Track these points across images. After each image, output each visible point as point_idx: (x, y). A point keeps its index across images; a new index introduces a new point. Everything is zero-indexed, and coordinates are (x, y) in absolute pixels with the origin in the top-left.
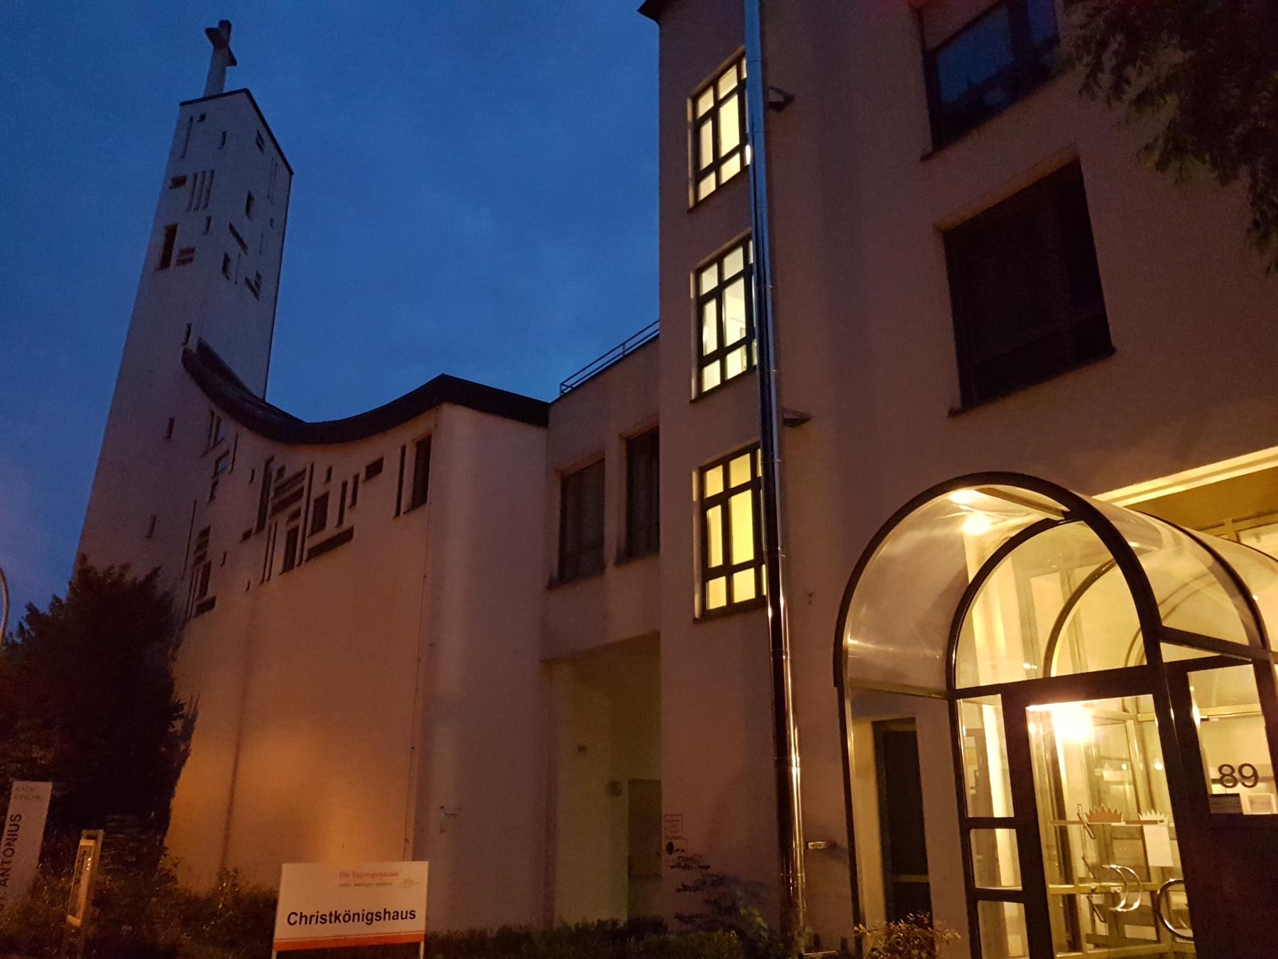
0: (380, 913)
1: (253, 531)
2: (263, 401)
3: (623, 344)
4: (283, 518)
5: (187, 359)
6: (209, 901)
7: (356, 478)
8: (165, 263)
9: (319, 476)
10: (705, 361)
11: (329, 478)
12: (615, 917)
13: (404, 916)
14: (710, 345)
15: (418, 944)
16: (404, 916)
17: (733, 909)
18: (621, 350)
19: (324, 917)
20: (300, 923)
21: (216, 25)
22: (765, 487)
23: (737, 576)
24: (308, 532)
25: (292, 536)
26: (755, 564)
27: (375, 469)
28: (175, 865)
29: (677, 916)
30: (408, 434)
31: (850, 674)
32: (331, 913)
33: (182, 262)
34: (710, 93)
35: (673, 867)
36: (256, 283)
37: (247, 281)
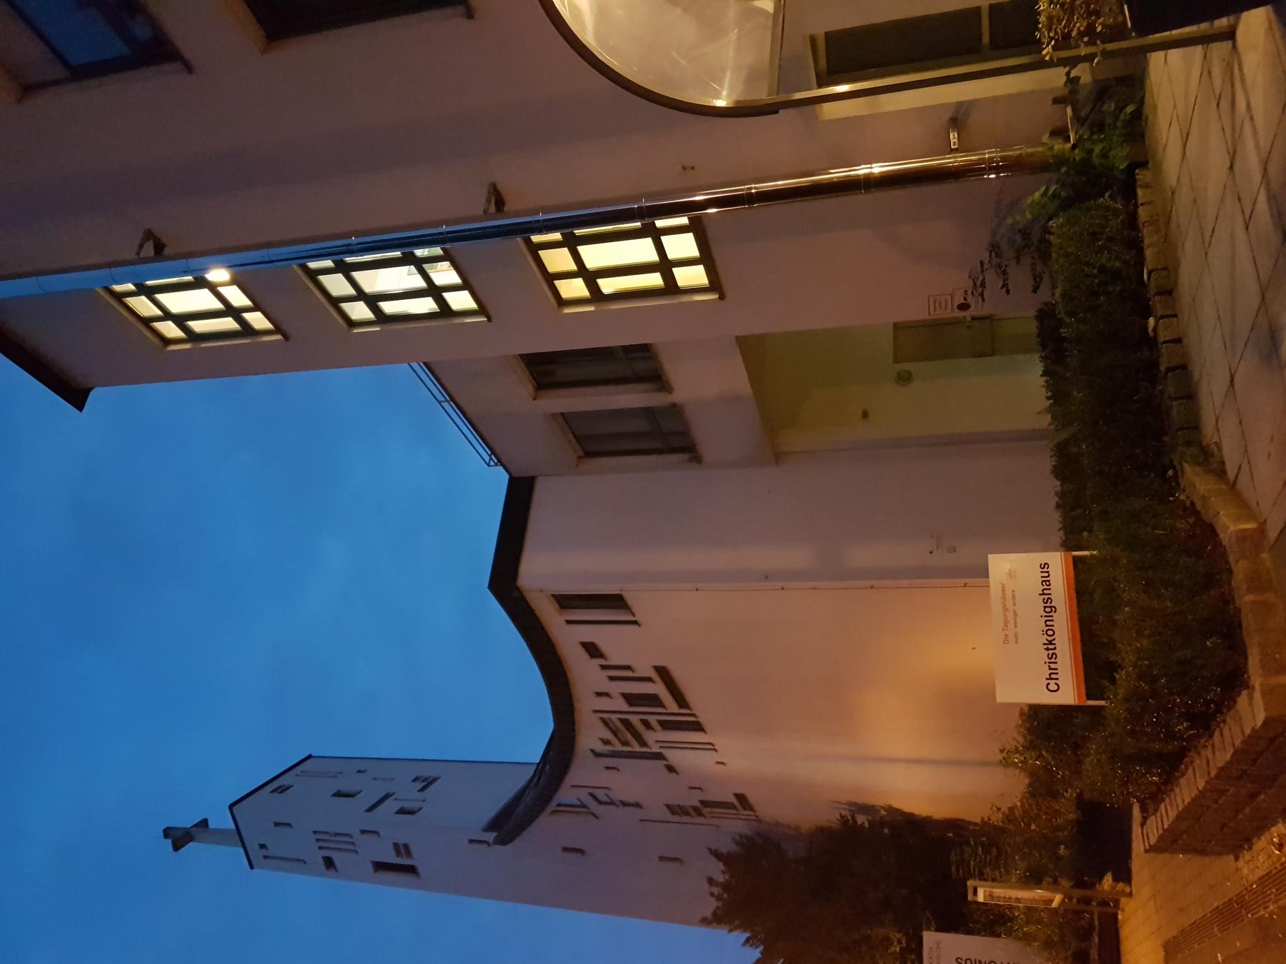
0: (1044, 599)
1: (666, 763)
2: (538, 764)
3: (440, 402)
4: (650, 737)
5: (503, 840)
6: (1032, 774)
7: (603, 667)
8: (411, 870)
9: (604, 704)
10: (445, 311)
11: (607, 695)
12: (1039, 362)
13: (1046, 574)
14: (426, 305)
15: (1074, 557)
16: (1046, 574)
17: (1025, 233)
18: (446, 405)
19: (1050, 656)
20: (1057, 679)
21: (169, 842)
22: (568, 228)
23: (672, 254)
25: (665, 725)
26: (656, 235)
27: (592, 650)
28: (999, 809)
29: (1035, 291)
30: (554, 620)
31: (762, 95)
32: (1045, 649)
34: (157, 325)
35: (983, 300)
36: (423, 781)
37: (422, 789)
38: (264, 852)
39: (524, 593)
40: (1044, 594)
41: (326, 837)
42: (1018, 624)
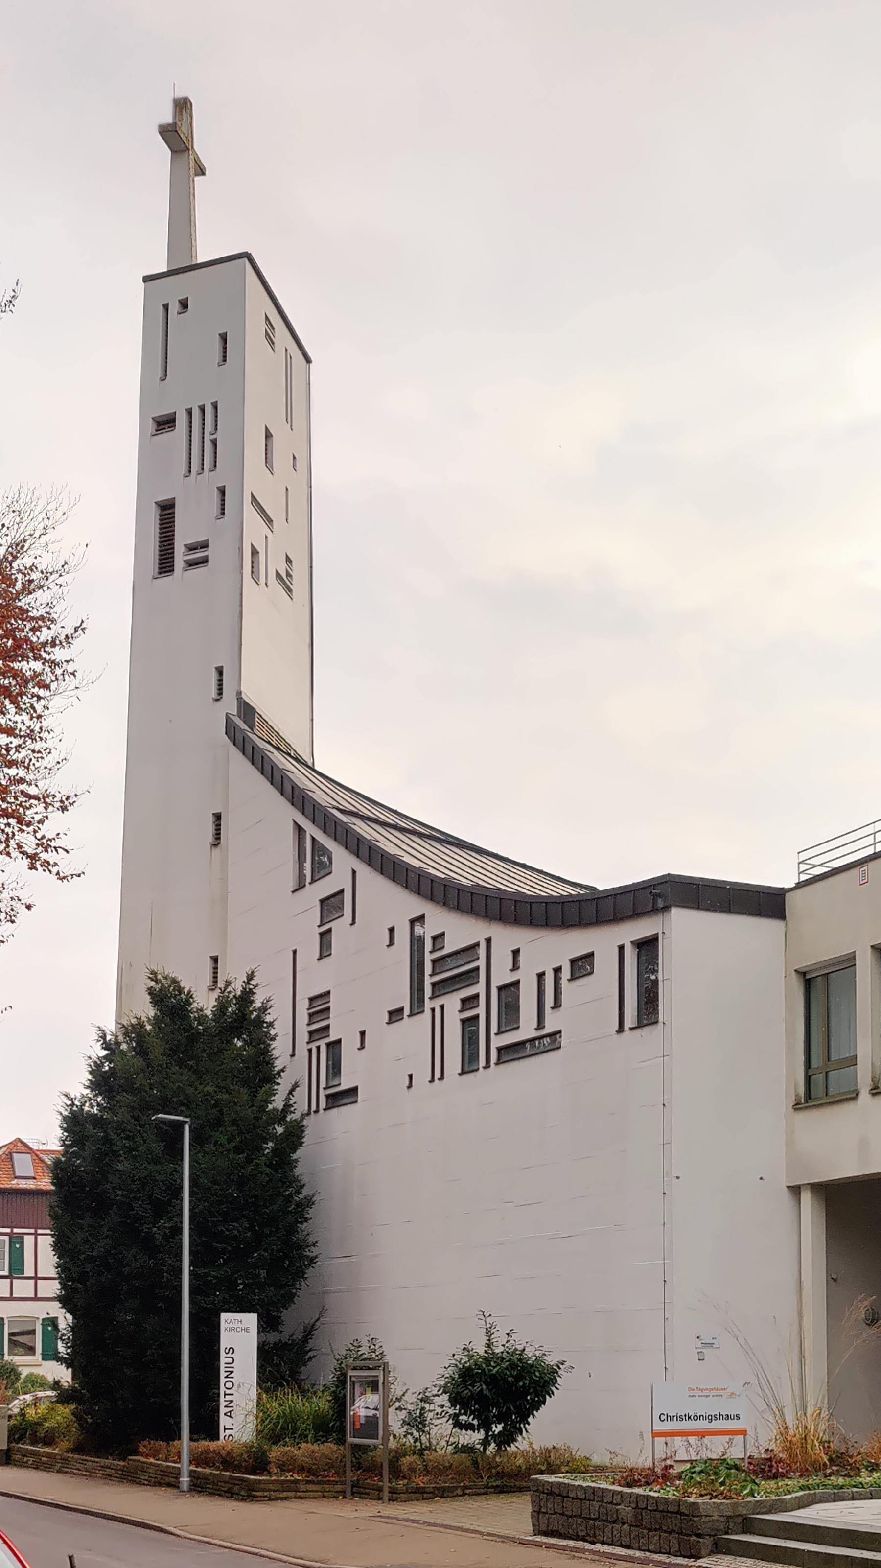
1: (407, 1011)
4: (452, 1002)
8: (166, 565)
24: (494, 1028)
33: (191, 564)
38: (174, 308)
39: (660, 916)
40: (720, 1415)
41: (209, 427)
42: (700, 1398)
